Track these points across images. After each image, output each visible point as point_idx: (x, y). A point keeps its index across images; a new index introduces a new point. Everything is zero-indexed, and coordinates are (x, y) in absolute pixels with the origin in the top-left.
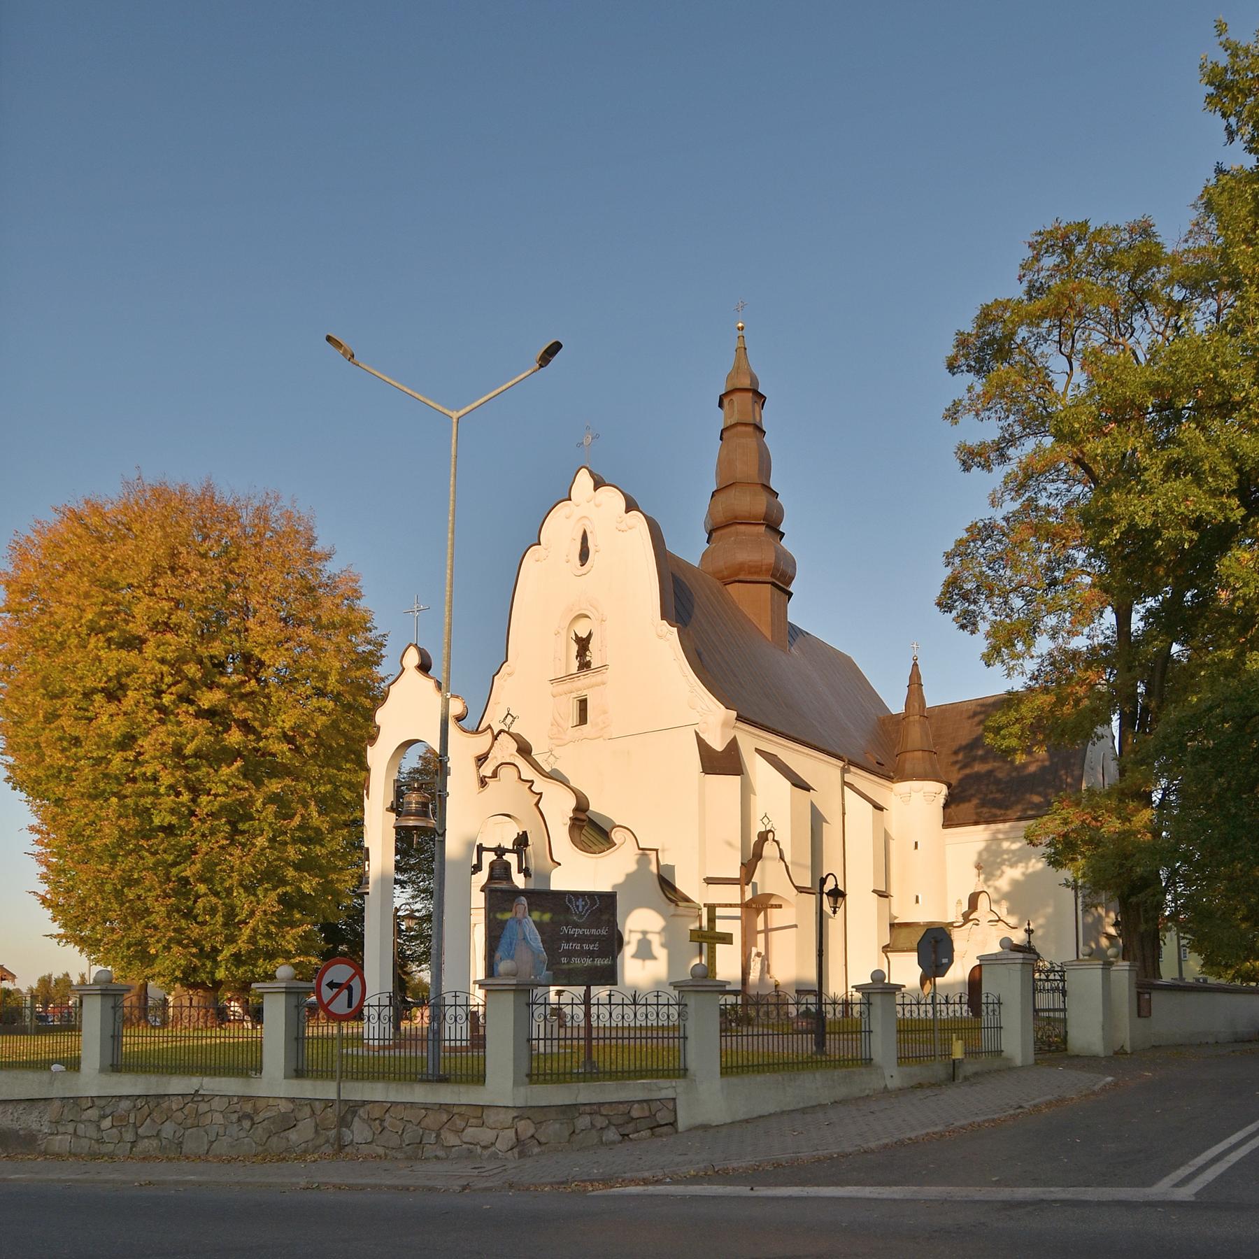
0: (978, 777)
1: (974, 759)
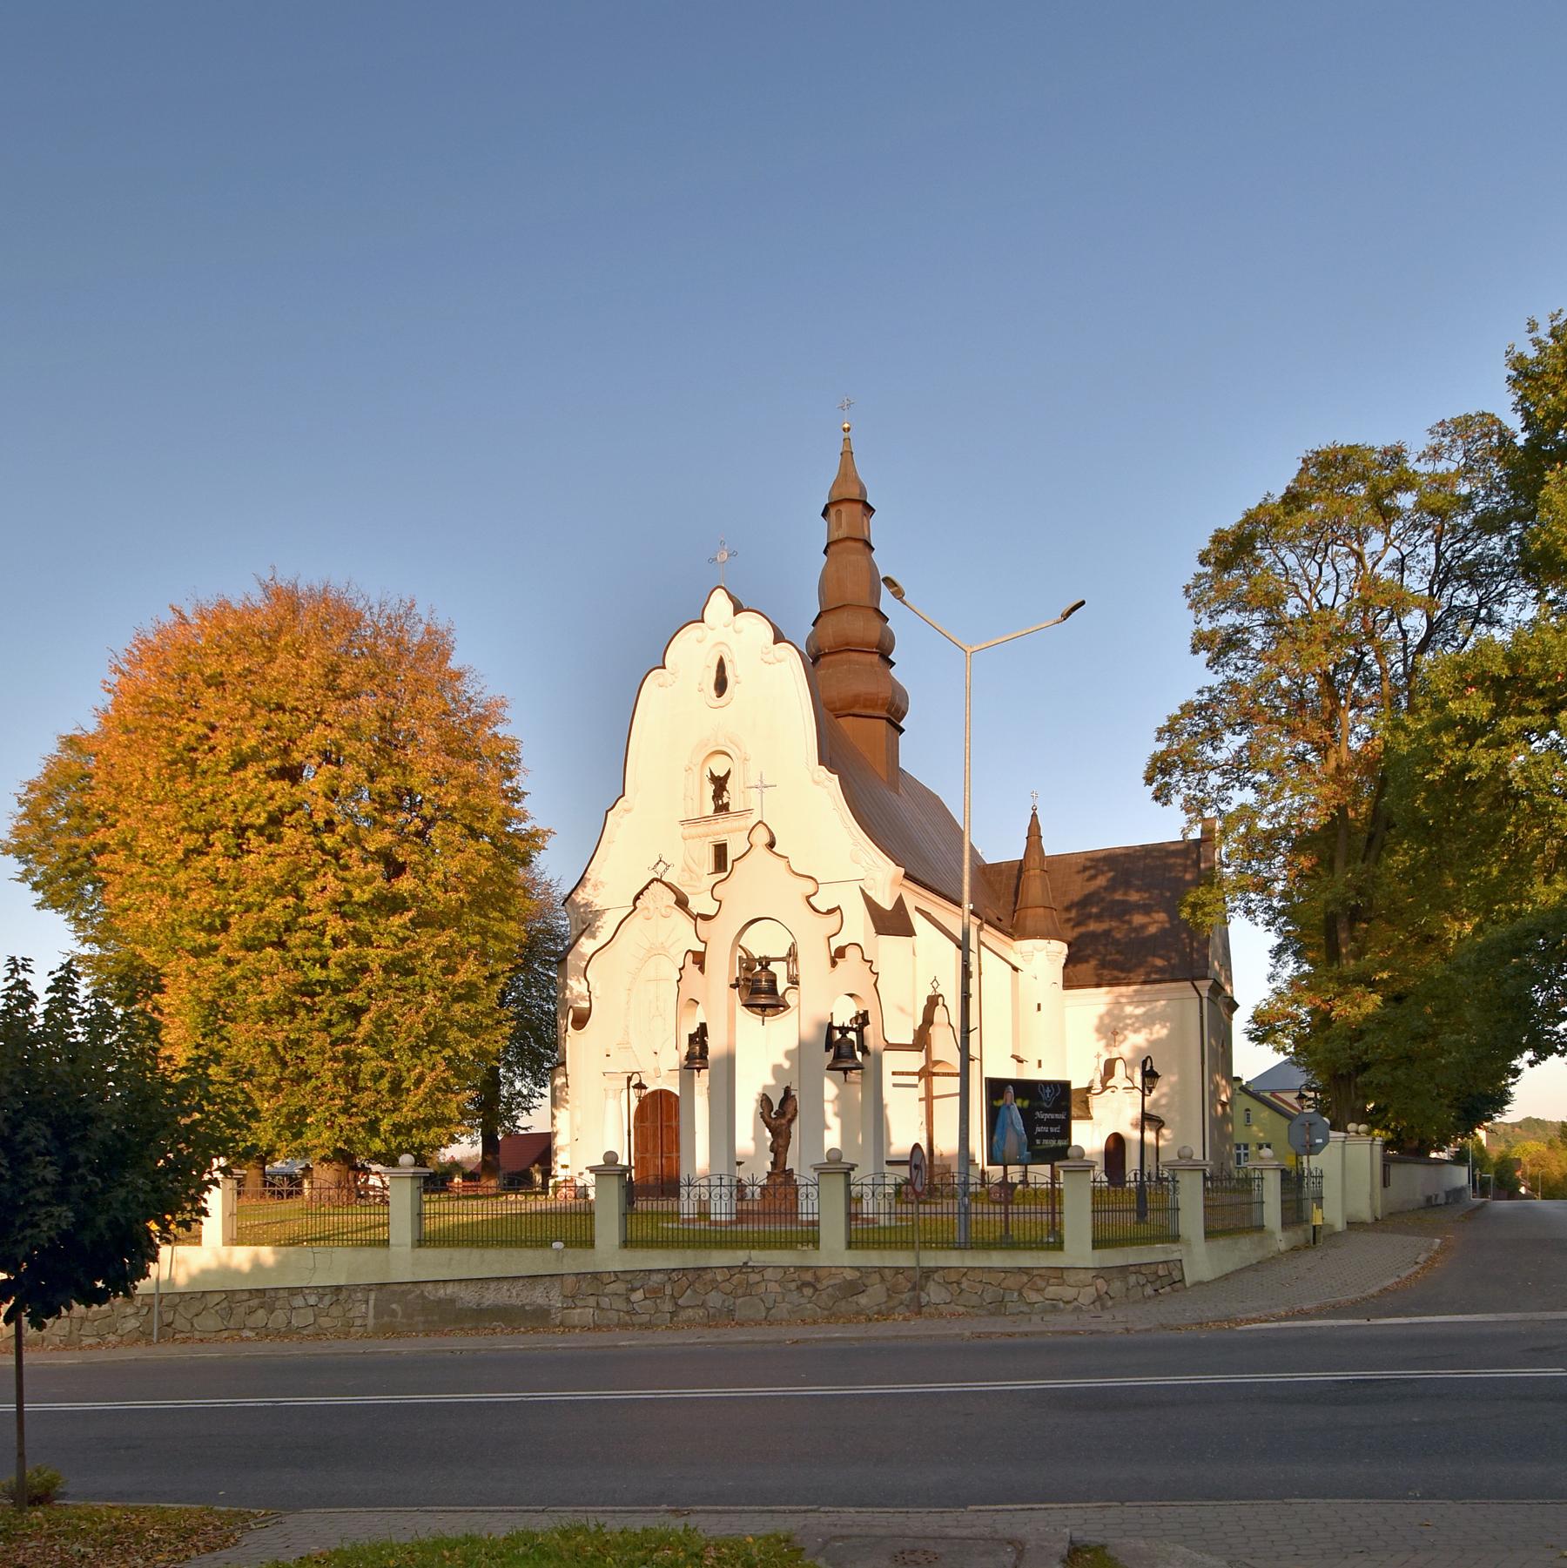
0: (1094, 936)
1: (1090, 916)
